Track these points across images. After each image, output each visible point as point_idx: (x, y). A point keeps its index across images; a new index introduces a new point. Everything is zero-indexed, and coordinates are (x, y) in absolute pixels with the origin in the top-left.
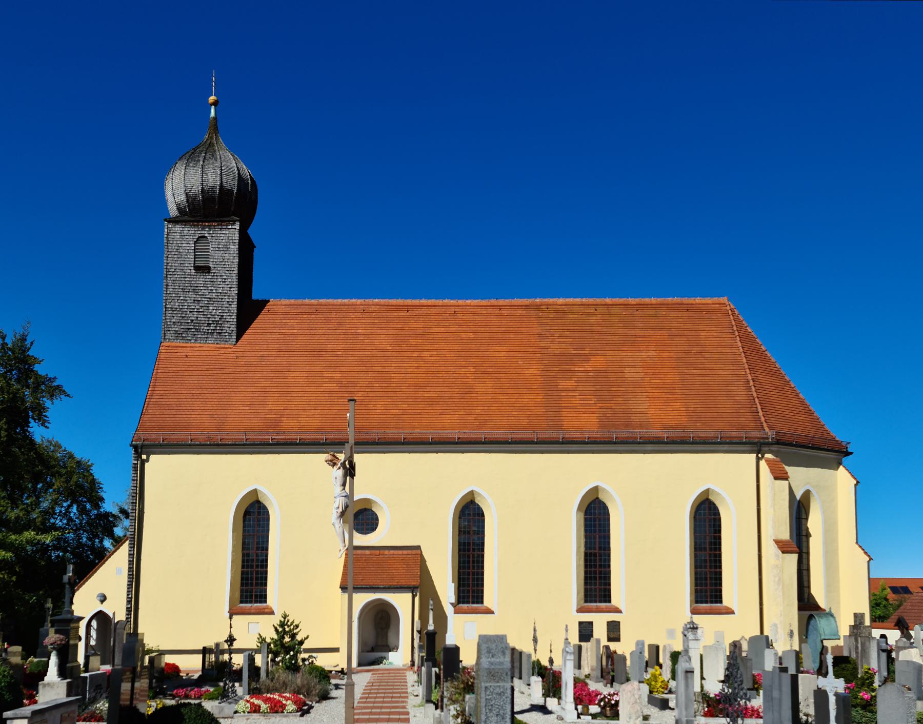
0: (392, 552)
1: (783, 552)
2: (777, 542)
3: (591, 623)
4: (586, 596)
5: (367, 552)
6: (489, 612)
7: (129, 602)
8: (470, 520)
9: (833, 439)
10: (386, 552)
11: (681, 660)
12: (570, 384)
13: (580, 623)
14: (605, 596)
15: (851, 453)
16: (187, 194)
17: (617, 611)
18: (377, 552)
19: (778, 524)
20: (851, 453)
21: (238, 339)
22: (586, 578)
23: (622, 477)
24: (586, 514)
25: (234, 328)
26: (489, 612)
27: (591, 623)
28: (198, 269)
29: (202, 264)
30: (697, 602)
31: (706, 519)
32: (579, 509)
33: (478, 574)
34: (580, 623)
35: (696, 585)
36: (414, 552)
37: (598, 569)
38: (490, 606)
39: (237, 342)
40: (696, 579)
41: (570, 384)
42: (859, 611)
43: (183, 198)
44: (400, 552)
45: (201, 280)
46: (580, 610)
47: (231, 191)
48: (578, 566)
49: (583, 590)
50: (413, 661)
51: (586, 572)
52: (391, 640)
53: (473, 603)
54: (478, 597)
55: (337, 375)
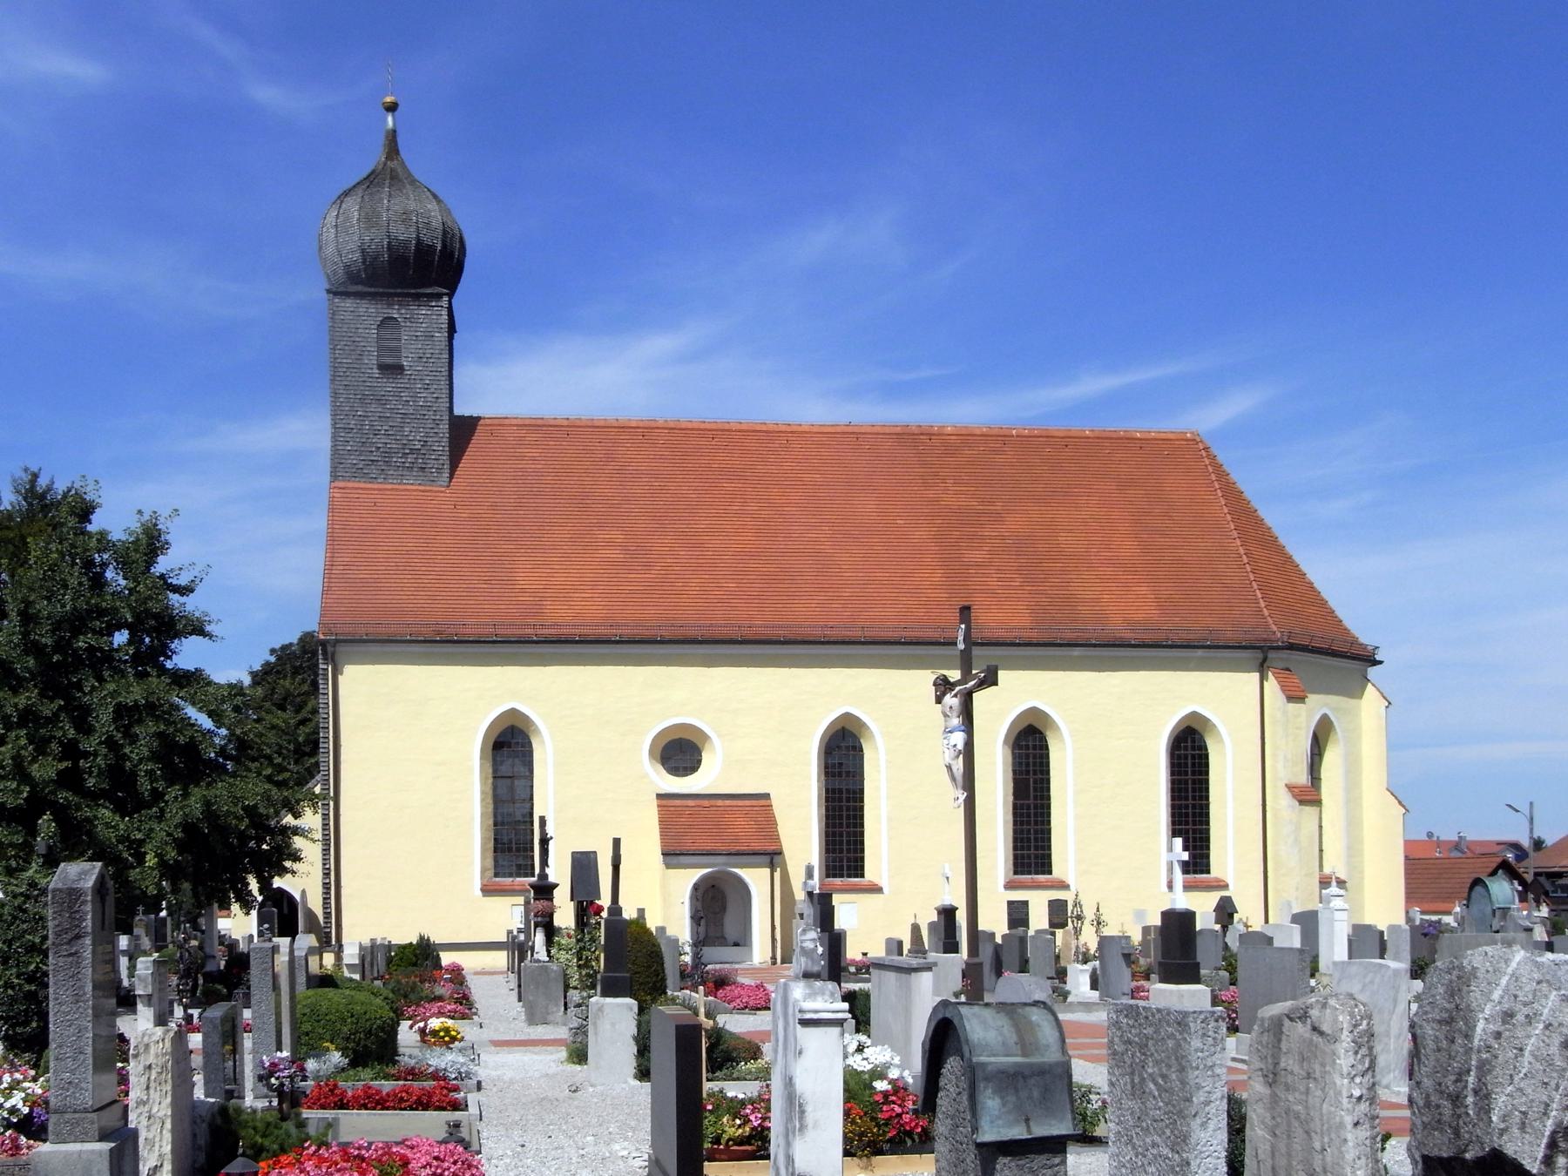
0: (728, 802)
1: (1301, 802)
2: (1290, 787)
3: (1026, 903)
4: (1015, 865)
5: (691, 803)
6: (875, 889)
7: (326, 875)
8: (843, 754)
9: (1354, 642)
10: (720, 803)
11: (1523, 935)
12: (978, 556)
13: (1010, 903)
14: (834, 868)
15: (1381, 662)
16: (363, 251)
17: (1064, 886)
18: (706, 803)
19: (1289, 764)
20: (1381, 662)
21: (451, 477)
22: (1015, 840)
23: (1068, 697)
24: (1013, 749)
25: (445, 458)
26: (875, 889)
27: (1026, 903)
28: (384, 368)
29: (389, 361)
30: (828, 876)
31: (1189, 755)
32: (1006, 742)
33: (1043, 832)
34: (1010, 903)
35: (827, 851)
36: (762, 802)
37: (1032, 827)
38: (876, 881)
39: (451, 477)
40: (827, 843)
41: (978, 556)
42: (948, 901)
43: (357, 256)
44: (740, 803)
45: (388, 386)
46: (1010, 886)
47: (432, 248)
48: (1005, 822)
49: (1011, 858)
50: (774, 958)
51: (1015, 832)
52: (730, 930)
53: (849, 876)
54: (856, 868)
55: (618, 536)
